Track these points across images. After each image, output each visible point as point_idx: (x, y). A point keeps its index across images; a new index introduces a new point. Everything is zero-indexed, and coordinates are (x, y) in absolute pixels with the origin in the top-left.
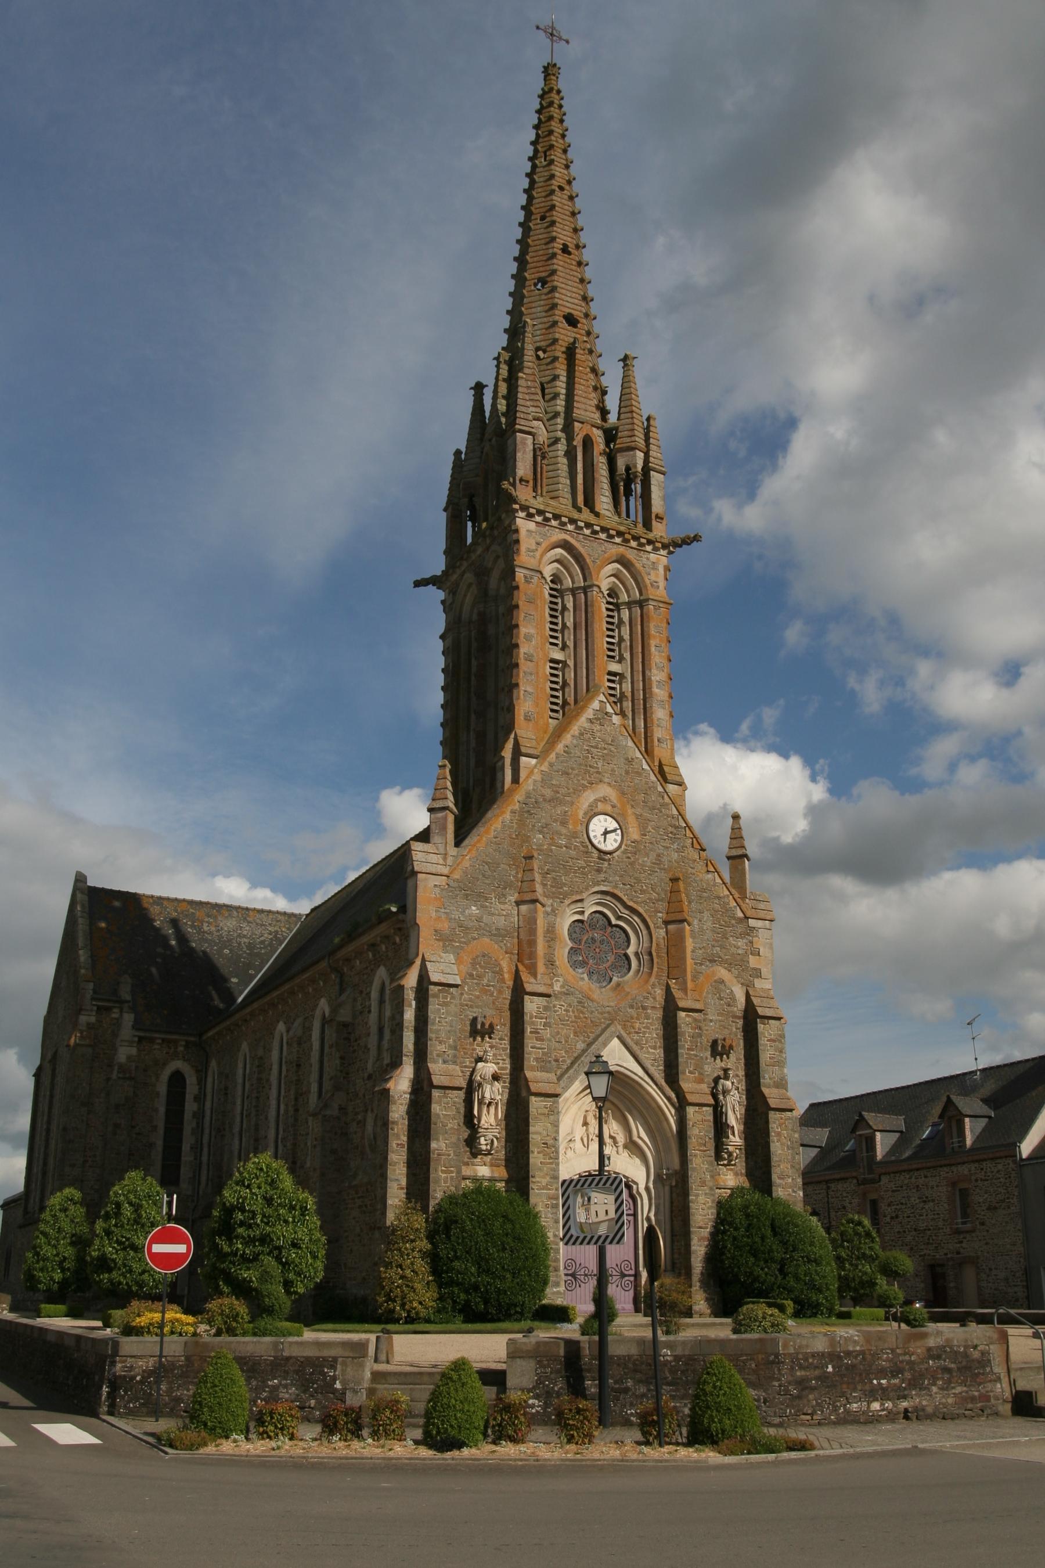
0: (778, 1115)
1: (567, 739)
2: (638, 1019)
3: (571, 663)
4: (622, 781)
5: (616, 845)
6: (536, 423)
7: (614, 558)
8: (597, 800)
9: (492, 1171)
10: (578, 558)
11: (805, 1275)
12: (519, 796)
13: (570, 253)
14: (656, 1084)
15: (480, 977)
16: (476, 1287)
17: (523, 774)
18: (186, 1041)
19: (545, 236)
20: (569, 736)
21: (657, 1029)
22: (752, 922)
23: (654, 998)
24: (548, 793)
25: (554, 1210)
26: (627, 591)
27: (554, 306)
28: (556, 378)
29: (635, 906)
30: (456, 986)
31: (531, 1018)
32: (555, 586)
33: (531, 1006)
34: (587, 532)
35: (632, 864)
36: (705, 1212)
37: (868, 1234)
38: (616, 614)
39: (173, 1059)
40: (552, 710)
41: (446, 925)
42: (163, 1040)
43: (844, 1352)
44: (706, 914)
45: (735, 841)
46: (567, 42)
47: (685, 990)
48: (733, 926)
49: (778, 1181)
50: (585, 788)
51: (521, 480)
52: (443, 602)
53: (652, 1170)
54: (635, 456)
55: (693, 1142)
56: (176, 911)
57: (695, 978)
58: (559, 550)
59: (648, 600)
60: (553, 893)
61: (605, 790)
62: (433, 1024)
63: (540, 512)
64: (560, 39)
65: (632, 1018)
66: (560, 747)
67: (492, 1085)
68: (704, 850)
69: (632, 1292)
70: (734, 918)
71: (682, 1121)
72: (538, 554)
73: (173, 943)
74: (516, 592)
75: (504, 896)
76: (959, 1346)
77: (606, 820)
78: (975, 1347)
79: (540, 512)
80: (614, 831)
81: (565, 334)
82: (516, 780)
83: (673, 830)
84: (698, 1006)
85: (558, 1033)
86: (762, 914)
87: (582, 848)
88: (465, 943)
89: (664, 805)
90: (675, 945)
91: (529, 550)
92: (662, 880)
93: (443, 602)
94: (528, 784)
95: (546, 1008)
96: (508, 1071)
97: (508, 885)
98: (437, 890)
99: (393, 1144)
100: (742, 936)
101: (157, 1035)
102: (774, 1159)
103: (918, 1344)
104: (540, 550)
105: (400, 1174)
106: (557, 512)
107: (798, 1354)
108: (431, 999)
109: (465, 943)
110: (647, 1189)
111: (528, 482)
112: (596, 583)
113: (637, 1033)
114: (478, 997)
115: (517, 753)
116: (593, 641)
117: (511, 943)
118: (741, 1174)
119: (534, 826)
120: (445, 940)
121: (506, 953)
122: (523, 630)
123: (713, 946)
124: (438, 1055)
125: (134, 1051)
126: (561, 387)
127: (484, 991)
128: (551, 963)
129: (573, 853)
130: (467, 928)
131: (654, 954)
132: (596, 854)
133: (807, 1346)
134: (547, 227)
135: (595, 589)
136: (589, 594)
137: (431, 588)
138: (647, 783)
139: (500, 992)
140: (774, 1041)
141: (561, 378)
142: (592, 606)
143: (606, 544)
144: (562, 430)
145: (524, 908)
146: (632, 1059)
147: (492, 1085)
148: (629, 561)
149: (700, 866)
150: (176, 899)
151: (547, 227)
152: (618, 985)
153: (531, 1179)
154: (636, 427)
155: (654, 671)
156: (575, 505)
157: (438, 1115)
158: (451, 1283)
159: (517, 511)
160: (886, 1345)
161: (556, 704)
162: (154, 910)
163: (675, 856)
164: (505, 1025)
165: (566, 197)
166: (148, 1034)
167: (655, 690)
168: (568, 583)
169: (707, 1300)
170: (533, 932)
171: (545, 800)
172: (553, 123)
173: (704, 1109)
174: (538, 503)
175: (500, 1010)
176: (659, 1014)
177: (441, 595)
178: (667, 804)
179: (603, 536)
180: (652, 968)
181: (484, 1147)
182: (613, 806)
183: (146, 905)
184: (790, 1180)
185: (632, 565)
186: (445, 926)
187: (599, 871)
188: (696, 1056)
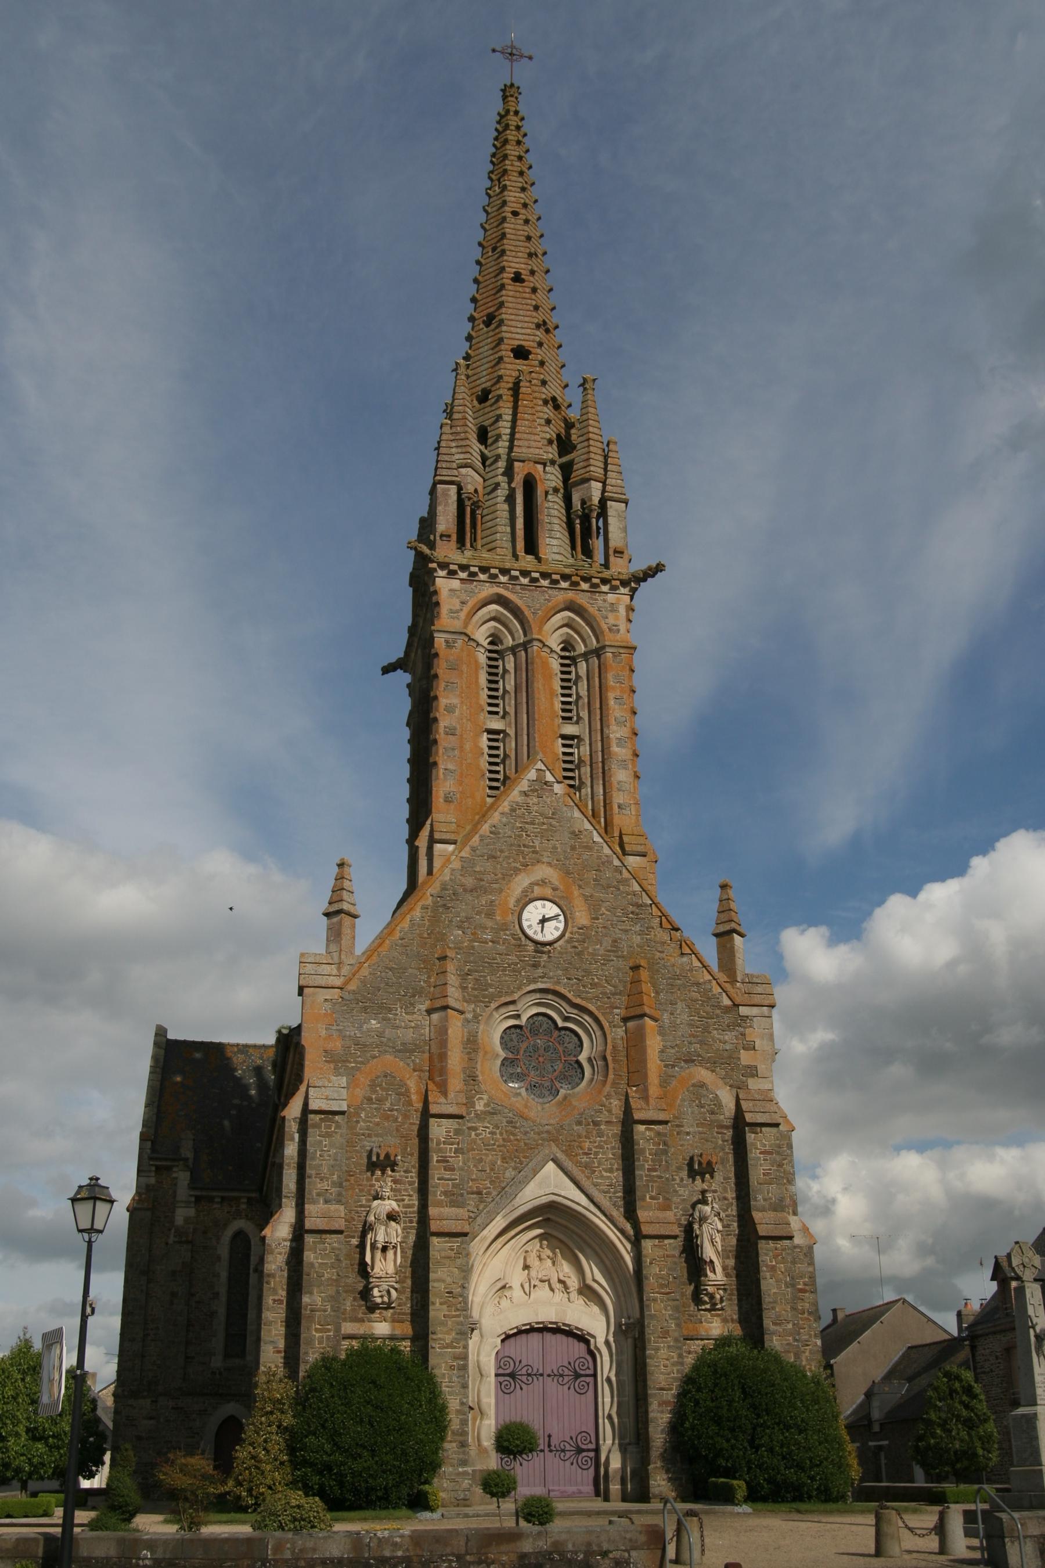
0: (771, 1244)
1: (496, 818)
3: (511, 732)
4: (566, 858)
5: (557, 934)
6: (463, 471)
7: (562, 606)
8: (532, 884)
9: (393, 1329)
10: (516, 612)
11: (782, 1447)
12: (434, 889)
13: (523, 281)
14: (605, 1215)
15: (380, 1100)
16: (329, 1468)
17: (437, 864)
18: (249, 1199)
19: (495, 268)
20: (497, 814)
21: (613, 1148)
22: (743, 1011)
23: (610, 1111)
24: (469, 881)
25: (461, 1373)
26: (584, 641)
27: (501, 341)
28: (499, 418)
29: (583, 1003)
30: (343, 1113)
32: (495, 648)
33: (438, 1130)
34: (525, 581)
35: (579, 954)
36: (669, 1369)
37: (968, 1390)
38: (573, 669)
39: (235, 1219)
40: (491, 788)
42: (223, 1198)
43: (374, 1559)
45: (722, 915)
46: (530, 58)
47: (646, 1098)
48: (718, 1016)
49: (772, 1327)
50: (517, 871)
51: (442, 536)
52: (408, 686)
53: (612, 1320)
54: (590, 488)
55: (651, 1282)
56: (261, 1058)
57: (664, 1083)
58: (494, 607)
59: (604, 647)
60: (476, 996)
61: (543, 871)
62: (313, 1158)
63: (464, 568)
64: (522, 56)
65: (579, 1136)
66: (485, 828)
67: (387, 1226)
68: (677, 930)
69: (592, 1470)
70: (719, 1007)
71: (638, 1259)
72: (463, 615)
73: (253, 1092)
74: (435, 661)
75: (412, 1004)
76: (576, 1553)
77: (544, 906)
78: (605, 1554)
79: (464, 568)
80: (555, 917)
81: (511, 368)
82: (430, 872)
83: (634, 909)
84: (662, 1116)
85: (481, 1160)
86: (757, 999)
87: (513, 942)
88: (362, 1063)
89: (625, 882)
90: (636, 1044)
91: (451, 611)
92: (619, 969)
93: (408, 686)
94: (444, 874)
95: (457, 1132)
96: (416, 1209)
97: (418, 992)
98: (328, 1005)
99: (269, 1300)
100: (730, 1027)
101: (215, 1194)
102: (766, 1300)
103: (504, 1548)
104: (466, 609)
105: (276, 1335)
106: (484, 564)
107: (297, 1559)
108: (310, 1130)
109: (362, 1063)
110: (607, 1343)
111: (449, 536)
112: (535, 636)
114: (378, 1124)
115: (432, 841)
116: (533, 703)
117: (421, 1059)
118: (733, 1320)
119: (451, 921)
120: (337, 1061)
121: (414, 1070)
122: (443, 701)
123: (690, 1043)
124: (318, 1195)
125: (192, 1212)
126: (504, 428)
127: (387, 1118)
128: (471, 1078)
129: (501, 948)
130: (365, 1046)
131: (609, 1058)
132: (531, 947)
133: (314, 1550)
134: (498, 258)
135: (535, 643)
136: (529, 650)
137: (399, 672)
138: (599, 858)
139: (406, 1117)
141: (505, 417)
142: (532, 663)
143: (550, 592)
144: (503, 474)
145: (435, 1016)
147: (387, 1226)
148: (581, 606)
149: (672, 949)
150: (264, 1046)
151: (498, 258)
152: (565, 1098)
153: (431, 1336)
154: (592, 455)
155: (614, 727)
156: (515, 556)
157: (312, 1264)
158: (305, 1463)
159: (435, 570)
160: (448, 1550)
161: (497, 780)
162: (238, 1059)
163: (637, 939)
164: (412, 1155)
165: (521, 222)
166: (204, 1193)
167: (615, 749)
168: (509, 642)
169: (670, 1480)
170: (443, 1043)
171: (465, 890)
172: (508, 147)
173: (666, 1241)
174: (457, 557)
175: (406, 1137)
176: (617, 1129)
177: (407, 678)
178: (627, 880)
179: (545, 583)
180: (606, 1075)
181: (379, 1300)
182: (555, 889)
183: (229, 1055)
184: (790, 1326)
185: (586, 610)
186: (337, 1045)
187: (536, 966)
188: (660, 1177)
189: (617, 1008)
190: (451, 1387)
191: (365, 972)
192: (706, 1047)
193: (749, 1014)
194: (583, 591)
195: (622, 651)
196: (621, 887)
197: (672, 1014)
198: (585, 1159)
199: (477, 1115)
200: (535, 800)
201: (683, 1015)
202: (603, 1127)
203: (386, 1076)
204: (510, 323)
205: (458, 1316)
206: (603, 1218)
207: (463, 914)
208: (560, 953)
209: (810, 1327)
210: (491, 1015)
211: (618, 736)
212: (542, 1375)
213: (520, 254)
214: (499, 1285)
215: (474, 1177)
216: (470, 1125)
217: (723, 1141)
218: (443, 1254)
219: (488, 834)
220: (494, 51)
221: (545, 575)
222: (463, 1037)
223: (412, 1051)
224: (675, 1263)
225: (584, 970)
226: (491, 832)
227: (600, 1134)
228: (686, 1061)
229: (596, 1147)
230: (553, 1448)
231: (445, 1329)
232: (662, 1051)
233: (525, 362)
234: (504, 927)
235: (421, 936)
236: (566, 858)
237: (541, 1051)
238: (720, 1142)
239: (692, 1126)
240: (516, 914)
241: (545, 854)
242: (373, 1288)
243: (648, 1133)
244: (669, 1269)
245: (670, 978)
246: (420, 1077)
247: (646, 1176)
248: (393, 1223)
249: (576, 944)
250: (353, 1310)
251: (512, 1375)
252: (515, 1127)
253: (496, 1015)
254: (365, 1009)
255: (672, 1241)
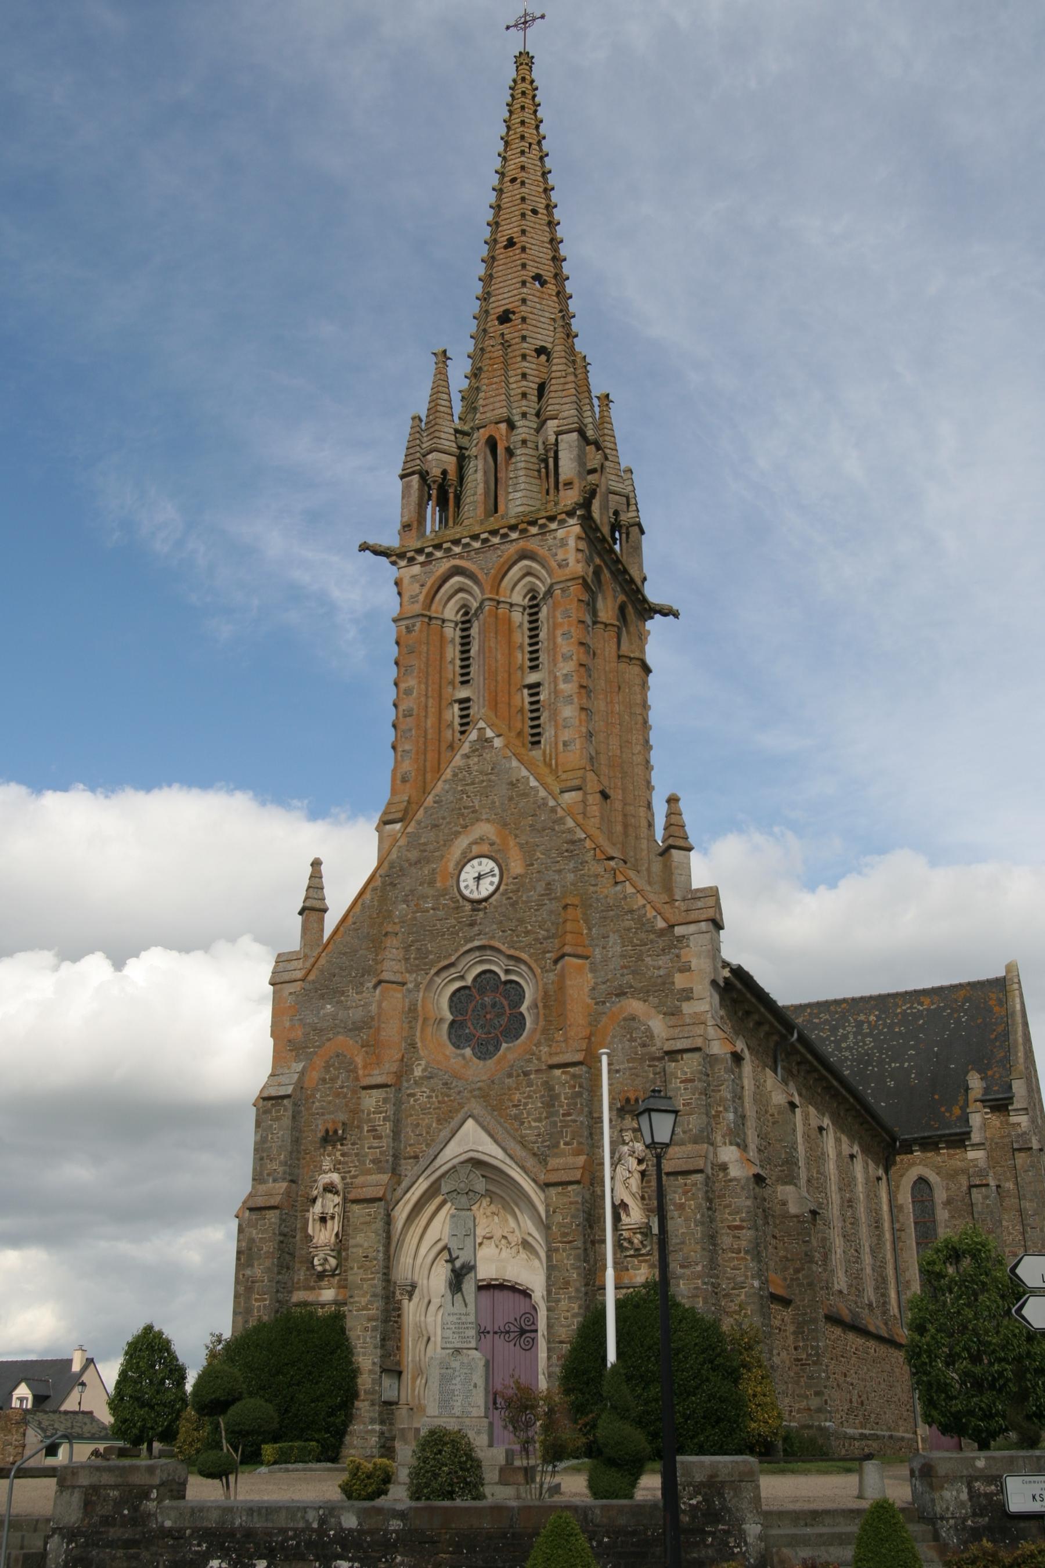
0: (681, 1180)
2: (517, 1089)
4: (504, 811)
5: (492, 889)
9: (337, 1295)
10: (471, 576)
15: (333, 1080)
21: (542, 1096)
23: (539, 1059)
24: (413, 855)
29: (517, 953)
30: (288, 1096)
31: (368, 1114)
34: (477, 545)
41: (300, 1033)
44: (613, 938)
46: (543, 17)
48: (652, 942)
50: (457, 834)
60: (417, 966)
61: (485, 829)
63: (420, 551)
64: (516, 26)
65: (509, 1089)
75: (362, 984)
79: (420, 551)
85: (418, 1125)
87: (453, 905)
88: (319, 1047)
91: (412, 597)
92: (551, 912)
98: (293, 997)
109: (319, 1047)
113: (515, 1106)
114: (330, 1102)
121: (363, 1047)
124: (269, 1175)
127: (337, 1095)
130: (321, 1030)
132: (468, 907)
140: (692, 1081)
143: (503, 547)
146: (488, 1139)
163: (570, 877)
171: (410, 865)
173: (570, 1188)
178: (562, 818)
179: (496, 540)
182: (492, 844)
187: (472, 924)
188: (575, 1121)
189: (549, 952)
190: (365, 1348)
191: (322, 961)
192: (638, 977)
193: (685, 933)
194: (534, 535)
195: (569, 584)
196: (557, 828)
197: (604, 948)
198: (514, 1111)
199: (416, 1082)
200: (476, 759)
201: (615, 945)
202: (532, 1076)
203: (338, 1056)
204: (497, 292)
205: (373, 1279)
206: (518, 1170)
207: (407, 888)
208: (495, 907)
209: (746, 1267)
210: (431, 981)
211: (565, 672)
212: (495, 1333)
213: (514, 219)
214: (440, 1245)
215: (412, 1142)
216: (409, 1092)
217: (655, 1074)
218: (362, 1220)
219: (432, 804)
220: (508, 28)
221: (513, 528)
222: (403, 1008)
223: (361, 1028)
224: (578, 1210)
225: (518, 920)
226: (435, 802)
227: (530, 1084)
228: (617, 995)
229: (525, 1098)
230: (498, 1406)
231: (361, 1292)
232: (594, 989)
233: (508, 325)
234: (444, 892)
235: (370, 917)
236: (504, 811)
237: (489, 1008)
238: (652, 1076)
239: (623, 1063)
240: (455, 877)
241: (484, 811)
242: (313, 1258)
243: (564, 1077)
244: (573, 1217)
245: (602, 911)
246: (367, 1052)
247: (561, 1121)
248: (329, 1195)
249: (511, 895)
250: (306, 1279)
251: (523, 1332)
252: (450, 1088)
253: (438, 980)
254: (322, 996)
255: (575, 1187)
